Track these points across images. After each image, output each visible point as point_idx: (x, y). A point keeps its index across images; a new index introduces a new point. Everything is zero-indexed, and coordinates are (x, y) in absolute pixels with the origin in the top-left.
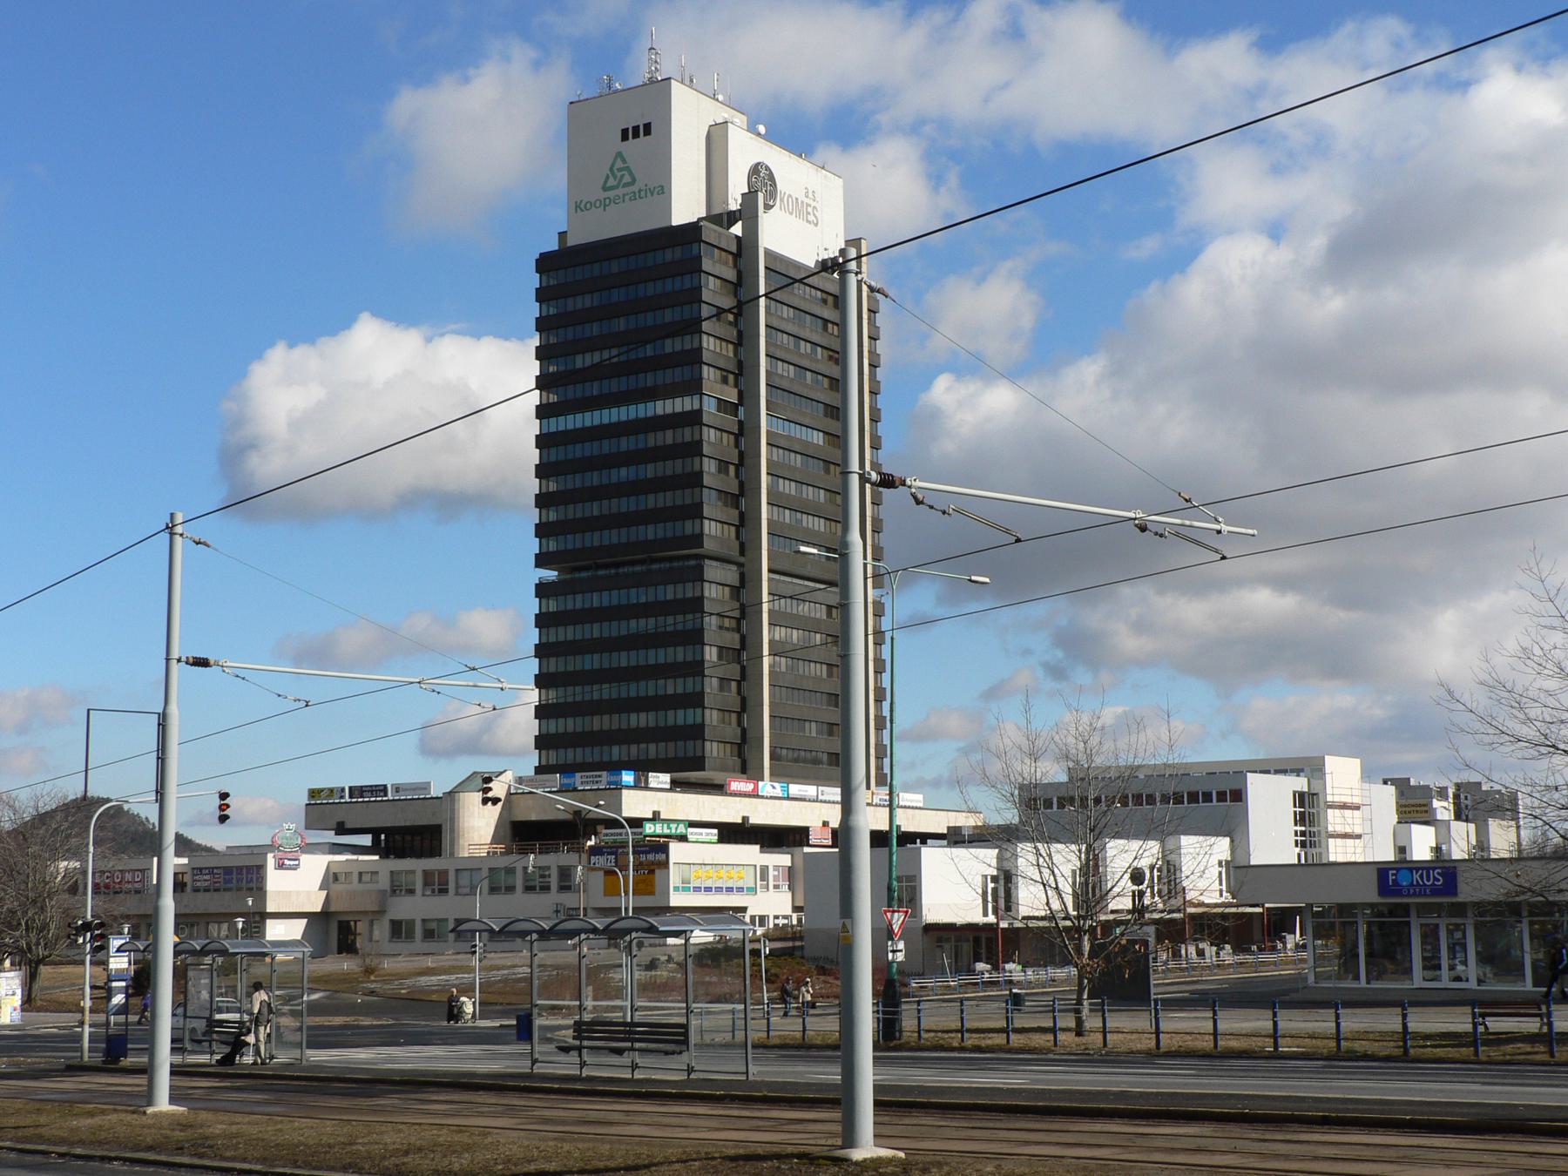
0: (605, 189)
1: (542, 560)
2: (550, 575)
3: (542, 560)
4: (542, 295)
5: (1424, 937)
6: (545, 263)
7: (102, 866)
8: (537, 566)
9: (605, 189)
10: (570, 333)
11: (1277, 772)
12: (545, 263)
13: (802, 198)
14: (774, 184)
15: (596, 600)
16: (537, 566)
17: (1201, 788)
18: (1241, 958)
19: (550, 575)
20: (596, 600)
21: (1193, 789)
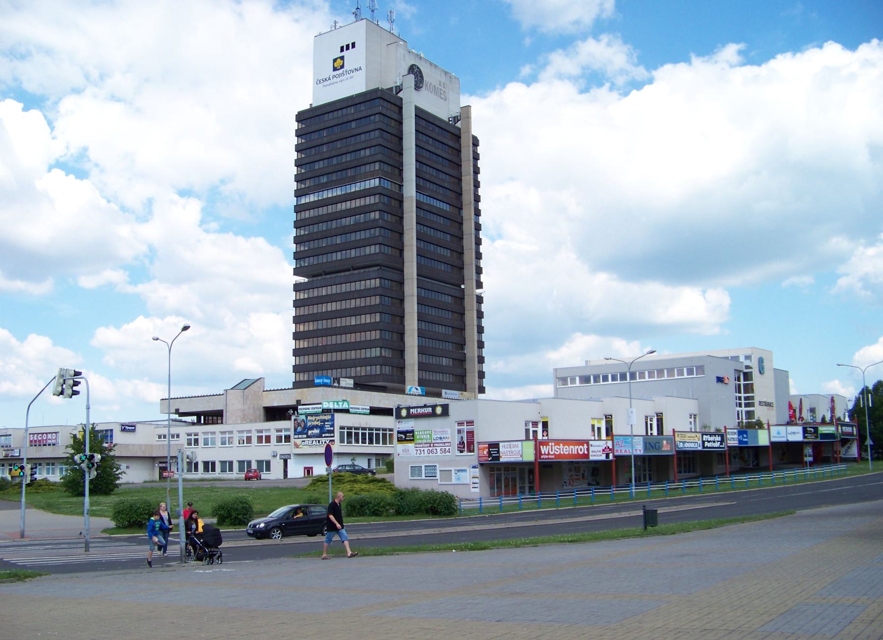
0: (335, 69)
1: (297, 272)
2: (302, 279)
3: (297, 272)
4: (299, 134)
5: (515, 504)
6: (301, 117)
7: (80, 499)
8: (295, 274)
9: (335, 69)
10: (312, 245)
11: (375, 555)
12: (301, 117)
13: (437, 86)
14: (422, 77)
15: (324, 292)
16: (295, 274)
17: (601, 372)
18: (507, 501)
19: (302, 279)
20: (324, 292)
21: (595, 373)
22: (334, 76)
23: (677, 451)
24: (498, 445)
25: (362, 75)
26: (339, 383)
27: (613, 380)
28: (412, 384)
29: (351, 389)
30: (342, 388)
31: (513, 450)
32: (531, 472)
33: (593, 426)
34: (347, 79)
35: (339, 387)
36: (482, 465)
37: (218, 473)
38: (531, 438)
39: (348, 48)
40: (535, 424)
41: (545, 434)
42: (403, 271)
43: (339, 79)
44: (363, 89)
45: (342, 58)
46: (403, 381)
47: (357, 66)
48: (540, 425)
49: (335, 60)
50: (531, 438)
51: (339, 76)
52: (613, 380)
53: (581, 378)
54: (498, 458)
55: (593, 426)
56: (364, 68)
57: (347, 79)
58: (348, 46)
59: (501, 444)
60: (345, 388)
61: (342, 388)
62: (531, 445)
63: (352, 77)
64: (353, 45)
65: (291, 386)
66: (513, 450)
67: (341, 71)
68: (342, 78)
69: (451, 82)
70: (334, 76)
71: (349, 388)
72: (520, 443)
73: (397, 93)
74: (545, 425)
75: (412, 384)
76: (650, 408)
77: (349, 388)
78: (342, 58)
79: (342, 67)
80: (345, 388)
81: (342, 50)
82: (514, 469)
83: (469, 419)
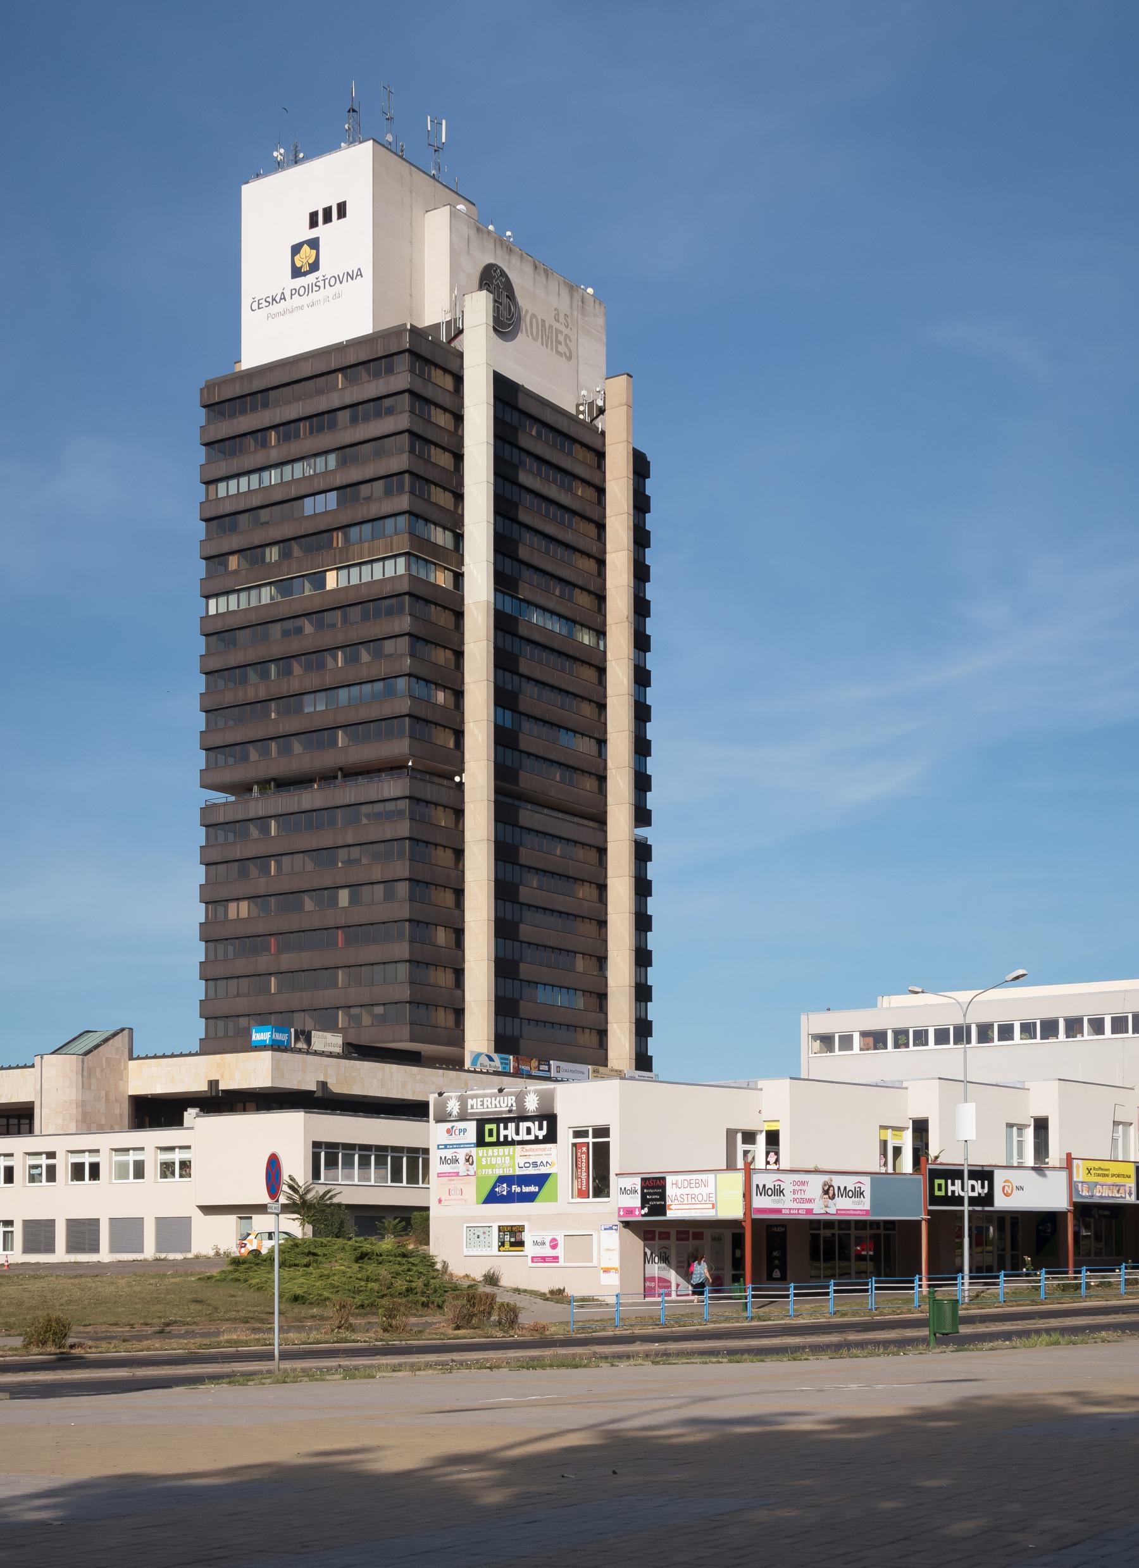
0: (297, 272)
9: (297, 272)
13: (550, 321)
14: (511, 296)
22: (295, 292)
23: (1076, 1205)
24: (664, 1179)
25: (364, 288)
26: (308, 1041)
27: (937, 1042)
28: (971, 1208)
29: (338, 1056)
30: (316, 1053)
31: (696, 1191)
32: (738, 1241)
33: (884, 1143)
34: (327, 299)
35: (308, 1053)
36: (627, 1224)
37: (60, 1255)
38: (740, 1164)
39: (328, 218)
40: (749, 1137)
41: (772, 1158)
42: (605, 823)
43: (306, 300)
44: (363, 326)
45: (314, 244)
46: (458, 1040)
47: (352, 268)
48: (761, 1139)
49: (296, 249)
50: (740, 1164)
51: (308, 290)
52: (937, 1042)
53: (864, 1034)
54: (661, 1210)
55: (884, 1143)
56: (368, 272)
57: (327, 299)
58: (327, 212)
59: (670, 1180)
60: (322, 1054)
61: (316, 1053)
62: (737, 1179)
63: (338, 296)
64: (342, 209)
65: (196, 1048)
66: (696, 1191)
67: (310, 279)
68: (314, 296)
69: (583, 311)
70: (295, 292)
71: (331, 1055)
72: (711, 1176)
73: (450, 342)
74: (773, 1138)
75: (971, 1208)
76: (804, 1040)
77: (331, 1055)
78: (314, 244)
79: (314, 267)
80: (322, 1054)
81: (313, 223)
82: (698, 1236)
83: (600, 1122)
